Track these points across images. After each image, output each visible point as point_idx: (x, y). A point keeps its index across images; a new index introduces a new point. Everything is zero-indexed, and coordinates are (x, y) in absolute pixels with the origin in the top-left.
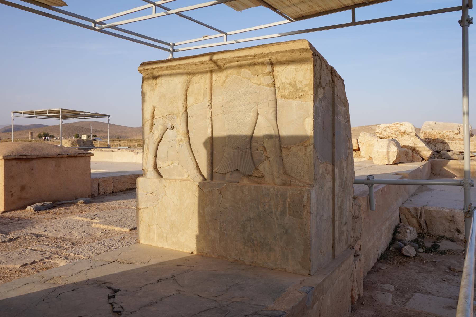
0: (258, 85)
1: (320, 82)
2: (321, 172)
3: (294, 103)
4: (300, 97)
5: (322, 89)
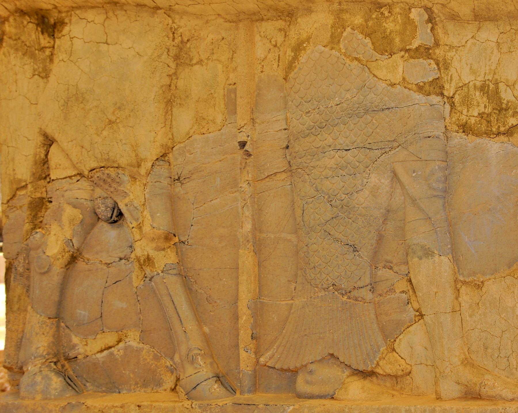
0: (393, 85)
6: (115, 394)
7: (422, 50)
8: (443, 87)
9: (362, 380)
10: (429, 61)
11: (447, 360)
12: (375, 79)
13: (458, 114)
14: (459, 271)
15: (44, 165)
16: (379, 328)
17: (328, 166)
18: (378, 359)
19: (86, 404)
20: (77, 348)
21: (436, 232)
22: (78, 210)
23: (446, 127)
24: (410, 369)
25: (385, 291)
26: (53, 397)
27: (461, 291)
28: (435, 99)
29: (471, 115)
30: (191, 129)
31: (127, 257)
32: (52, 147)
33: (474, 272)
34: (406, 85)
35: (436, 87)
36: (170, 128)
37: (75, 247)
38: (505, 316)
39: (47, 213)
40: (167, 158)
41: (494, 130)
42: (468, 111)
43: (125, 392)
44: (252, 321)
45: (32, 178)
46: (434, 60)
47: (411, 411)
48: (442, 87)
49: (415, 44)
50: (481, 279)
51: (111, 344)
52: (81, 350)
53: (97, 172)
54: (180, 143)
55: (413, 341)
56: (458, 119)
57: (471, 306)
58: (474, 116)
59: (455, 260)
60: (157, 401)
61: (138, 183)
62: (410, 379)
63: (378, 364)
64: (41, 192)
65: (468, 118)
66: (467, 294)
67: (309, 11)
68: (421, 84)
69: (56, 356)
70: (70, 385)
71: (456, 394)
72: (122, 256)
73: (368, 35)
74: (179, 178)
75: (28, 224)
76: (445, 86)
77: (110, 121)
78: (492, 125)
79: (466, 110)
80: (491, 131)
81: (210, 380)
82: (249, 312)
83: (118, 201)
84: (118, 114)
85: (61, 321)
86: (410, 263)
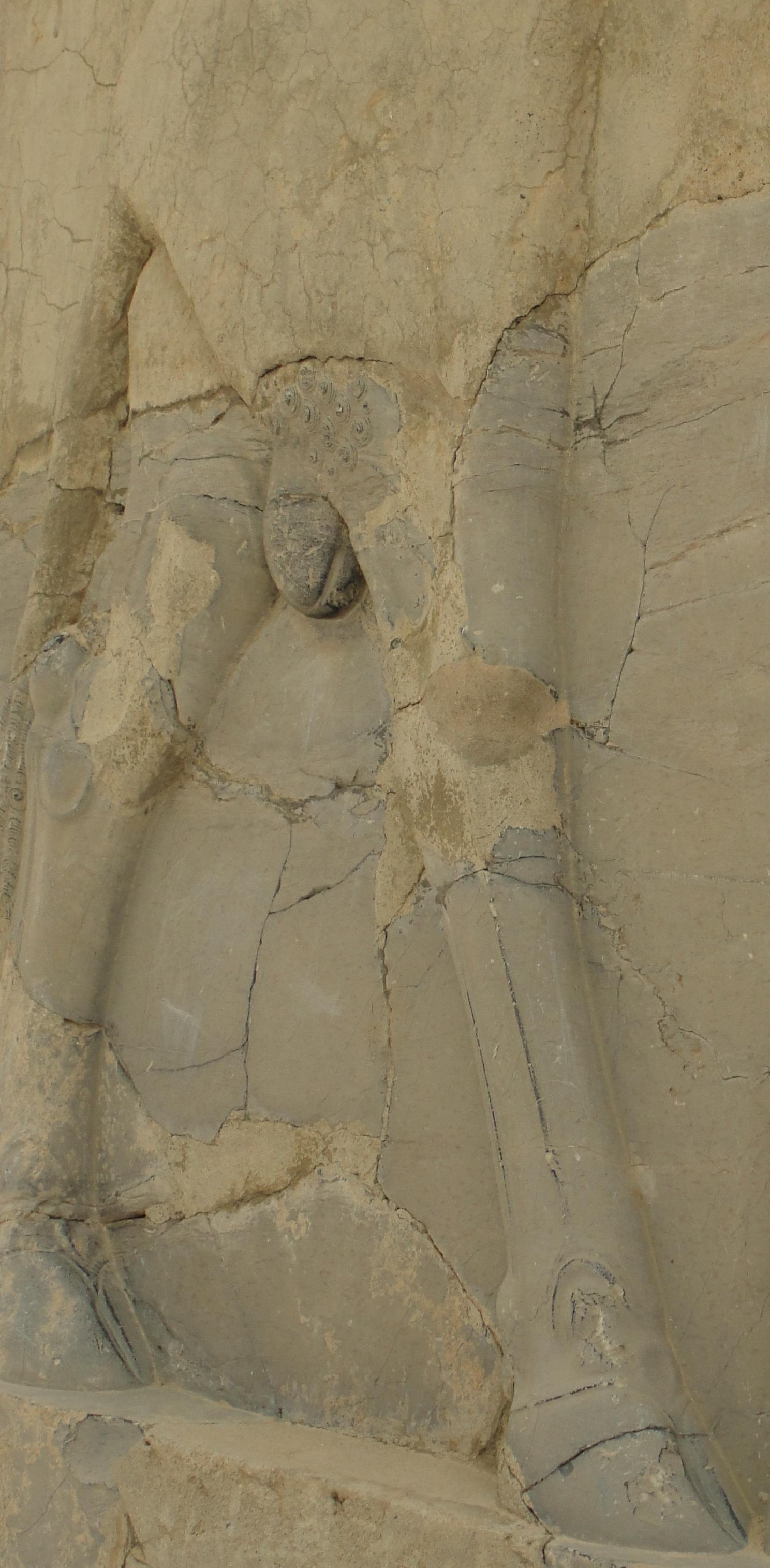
6: (259, 1416)
15: (111, 350)
19: (147, 1435)
20: (149, 1172)
22: (204, 546)
26: (42, 1375)
30: (669, 174)
31: (364, 779)
32: (147, 269)
36: (584, 173)
37: (183, 718)
39: (104, 556)
40: (556, 319)
43: (299, 1415)
45: (67, 406)
51: (269, 1178)
52: (161, 1186)
53: (285, 379)
54: (618, 244)
60: (409, 1493)
61: (431, 435)
64: (90, 464)
69: (74, 1193)
70: (106, 1335)
72: (347, 777)
74: (598, 418)
75: (36, 599)
77: (355, 144)
81: (638, 1441)
83: (349, 517)
84: (385, 111)
85: (106, 1040)
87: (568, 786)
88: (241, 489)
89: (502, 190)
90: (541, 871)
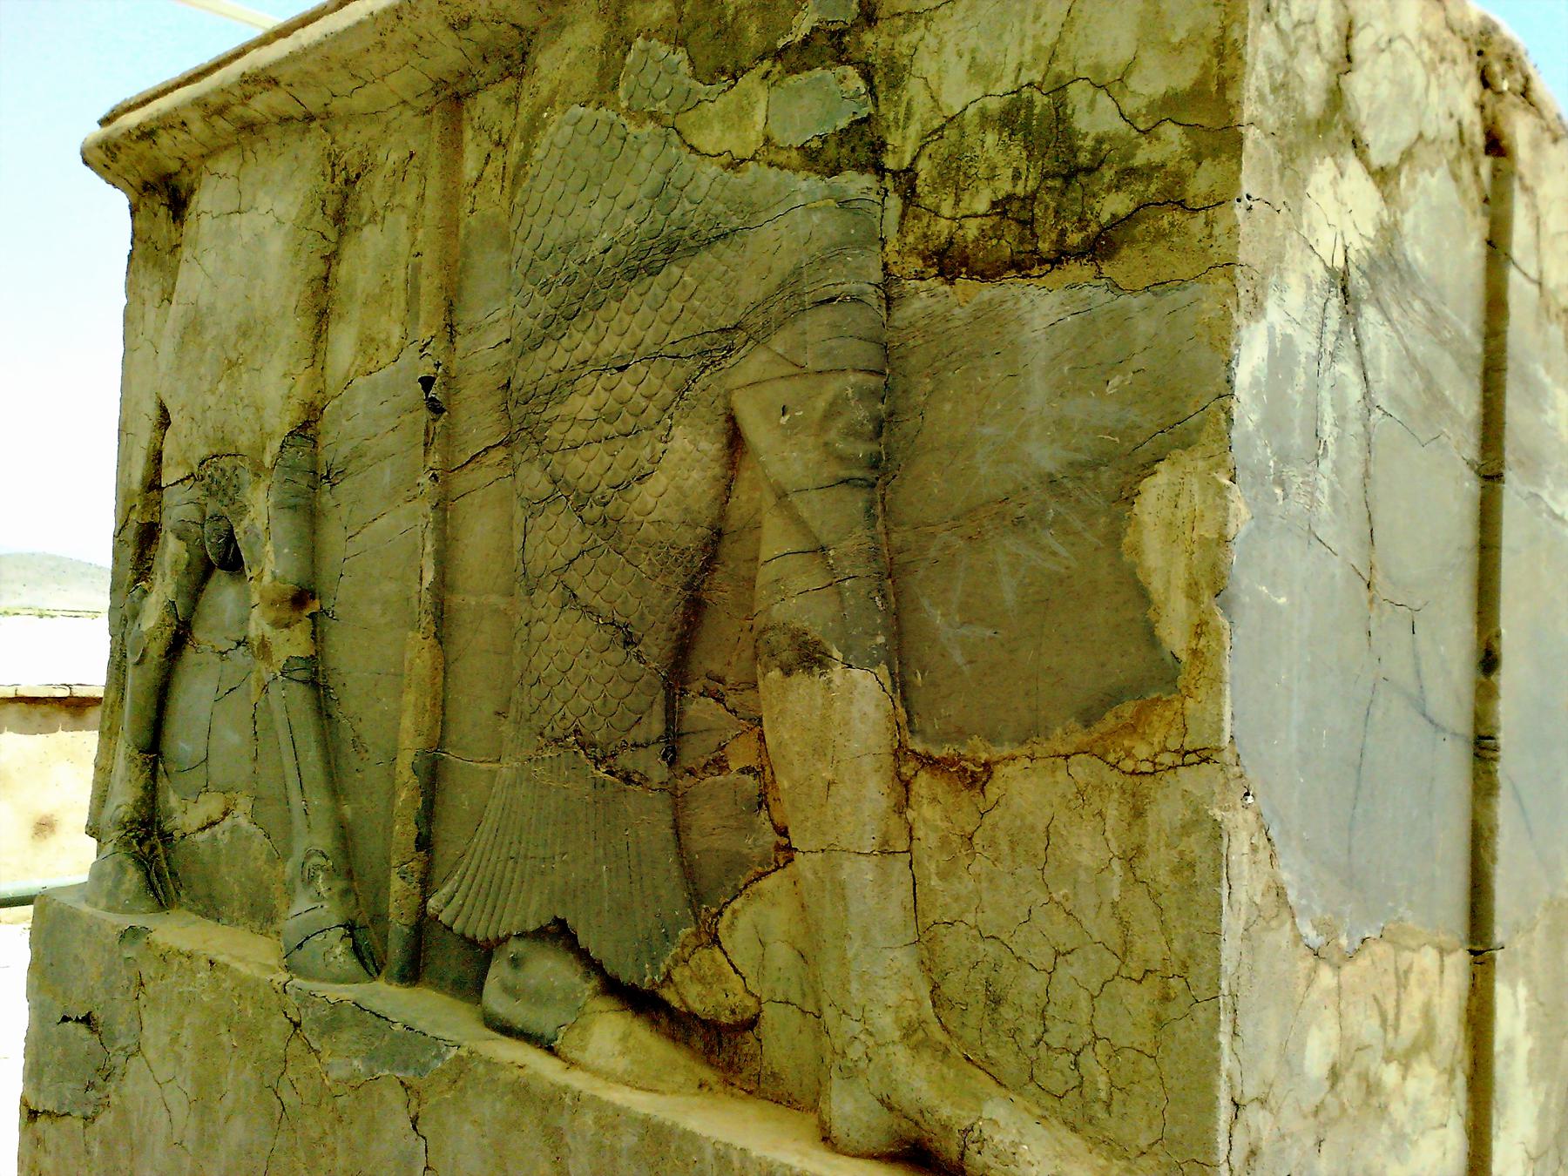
0: (736, 164)
1: (1336, 98)
2: (1317, 1053)
3: (1041, 307)
4: (1102, 246)
5: (1359, 186)
7: (822, 40)
8: (884, 144)
9: (629, 1013)
10: (840, 70)
11: (856, 1014)
12: (694, 156)
13: (925, 220)
14: (910, 721)
16: (682, 864)
17: (580, 416)
18: (668, 960)
21: (839, 593)
23: (885, 266)
24: (754, 1011)
25: (703, 762)
27: (915, 787)
28: (856, 183)
29: (965, 215)
33: (960, 731)
34: (771, 157)
35: (861, 144)
38: (1065, 896)
40: (310, 432)
41: (1044, 246)
42: (957, 203)
44: (420, 805)
46: (856, 64)
47: (731, 1162)
48: (879, 147)
49: (803, 25)
50: (984, 757)
51: (216, 816)
52: (178, 822)
54: (334, 397)
55: (759, 924)
56: (925, 236)
57: (944, 842)
58: (976, 216)
59: (901, 687)
62: (753, 1040)
63: (669, 976)
65: (955, 225)
66: (934, 800)
67: (560, 26)
68: (816, 144)
71: (878, 1141)
73: (681, 42)
76: (889, 141)
78: (1038, 231)
79: (951, 200)
80: (1034, 252)
82: (415, 781)
86: (760, 683)
87: (316, 636)
88: (197, 517)
89: (285, 375)
90: (303, 675)
